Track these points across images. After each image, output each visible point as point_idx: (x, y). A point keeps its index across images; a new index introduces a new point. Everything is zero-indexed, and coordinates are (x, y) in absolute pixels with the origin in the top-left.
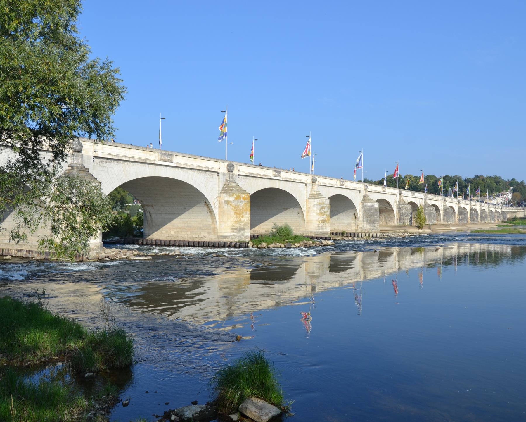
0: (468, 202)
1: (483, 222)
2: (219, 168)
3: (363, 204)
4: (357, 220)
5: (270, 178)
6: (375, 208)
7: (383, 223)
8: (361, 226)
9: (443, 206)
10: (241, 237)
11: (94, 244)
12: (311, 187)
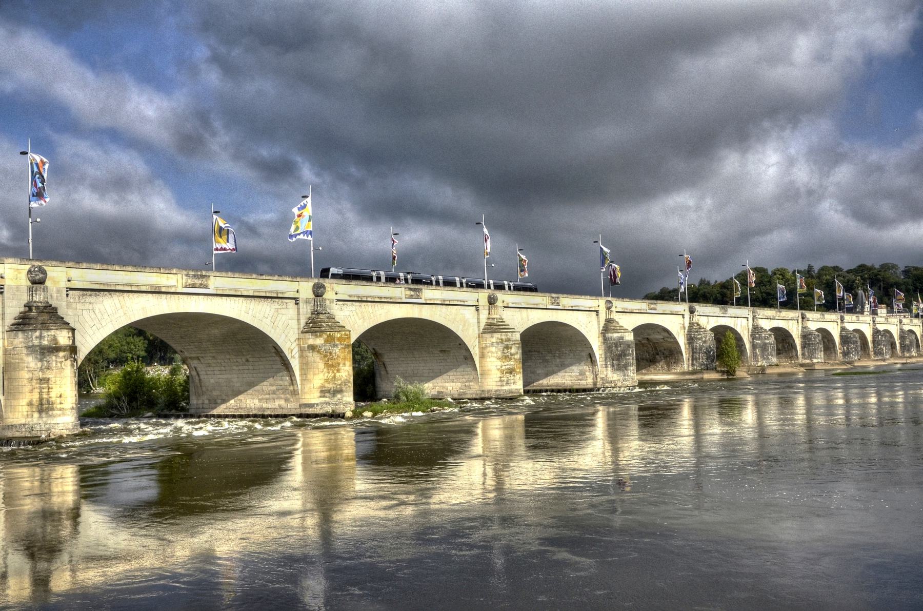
0: (894, 320)
1: (907, 355)
2: (297, 292)
3: (604, 336)
4: (595, 366)
5: (399, 301)
6: (627, 341)
7: (662, 367)
8: (603, 376)
9: (800, 328)
10: (336, 404)
11: (62, 425)
12: (486, 312)
